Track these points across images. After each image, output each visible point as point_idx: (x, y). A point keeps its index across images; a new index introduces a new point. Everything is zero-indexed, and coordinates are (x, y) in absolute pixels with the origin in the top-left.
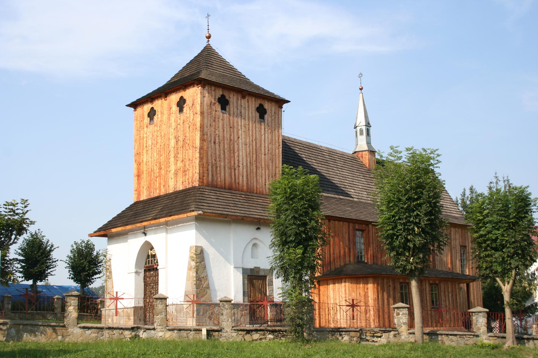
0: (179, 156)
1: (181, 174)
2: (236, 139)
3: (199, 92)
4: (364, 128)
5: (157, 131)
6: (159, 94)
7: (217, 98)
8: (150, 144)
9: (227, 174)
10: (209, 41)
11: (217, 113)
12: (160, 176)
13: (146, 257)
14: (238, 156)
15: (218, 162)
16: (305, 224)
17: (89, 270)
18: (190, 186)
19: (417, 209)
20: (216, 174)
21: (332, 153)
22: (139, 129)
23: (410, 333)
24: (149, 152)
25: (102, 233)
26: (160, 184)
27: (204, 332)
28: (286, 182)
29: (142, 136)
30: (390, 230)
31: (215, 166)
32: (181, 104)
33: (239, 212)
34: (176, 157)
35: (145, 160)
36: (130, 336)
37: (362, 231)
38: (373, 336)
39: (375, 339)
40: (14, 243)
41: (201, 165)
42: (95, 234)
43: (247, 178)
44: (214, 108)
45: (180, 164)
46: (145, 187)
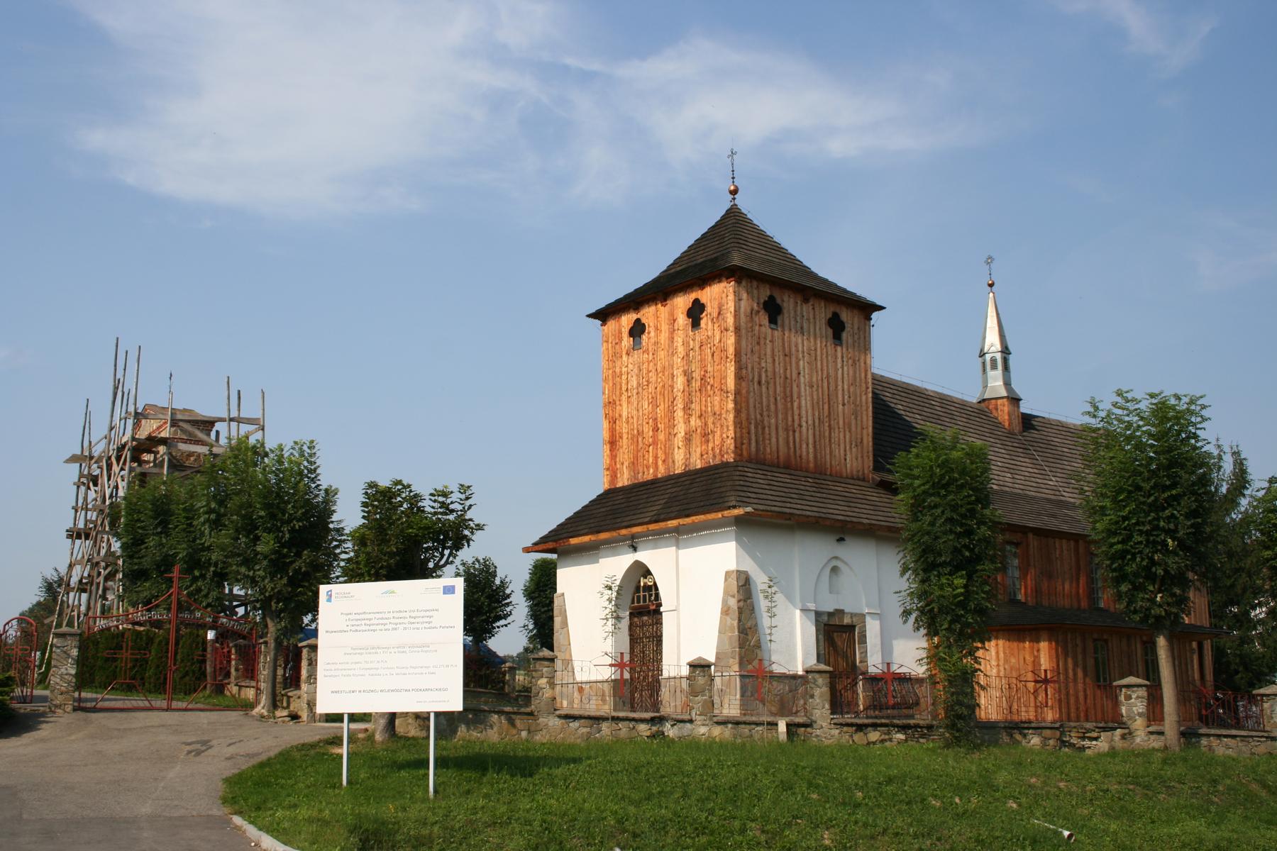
0: (693, 406)
1: (694, 439)
2: (794, 376)
3: (731, 290)
4: (999, 356)
5: (649, 362)
8: (635, 384)
9: (781, 440)
11: (763, 329)
12: (655, 443)
13: (632, 590)
14: (800, 407)
16: (969, 533)
17: (490, 611)
18: (717, 461)
19: (1172, 506)
20: (764, 440)
21: (945, 401)
22: (614, 357)
23: (1151, 733)
24: (634, 399)
25: (551, 545)
26: (656, 458)
27: (782, 727)
28: (933, 456)
29: (618, 370)
30: (1119, 543)
31: (760, 425)
32: (696, 312)
33: (810, 510)
34: (687, 409)
35: (625, 414)
36: (648, 733)
37: (1017, 545)
38: (1083, 738)
39: (1087, 743)
40: (447, 563)
41: (738, 423)
42: (537, 548)
43: (815, 447)
44: (756, 319)
45: (695, 422)
46: (626, 464)
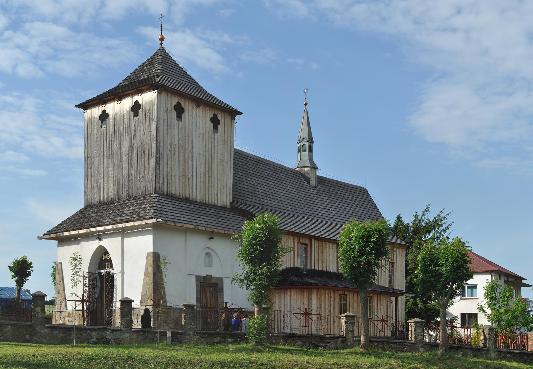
6: (113, 97)
7: (173, 105)
10: (162, 43)
15: (173, 171)
42: (47, 236)
